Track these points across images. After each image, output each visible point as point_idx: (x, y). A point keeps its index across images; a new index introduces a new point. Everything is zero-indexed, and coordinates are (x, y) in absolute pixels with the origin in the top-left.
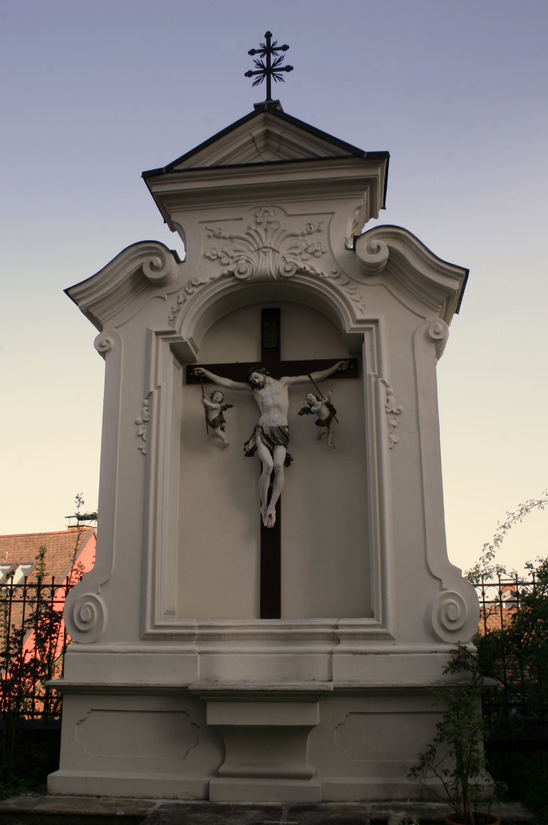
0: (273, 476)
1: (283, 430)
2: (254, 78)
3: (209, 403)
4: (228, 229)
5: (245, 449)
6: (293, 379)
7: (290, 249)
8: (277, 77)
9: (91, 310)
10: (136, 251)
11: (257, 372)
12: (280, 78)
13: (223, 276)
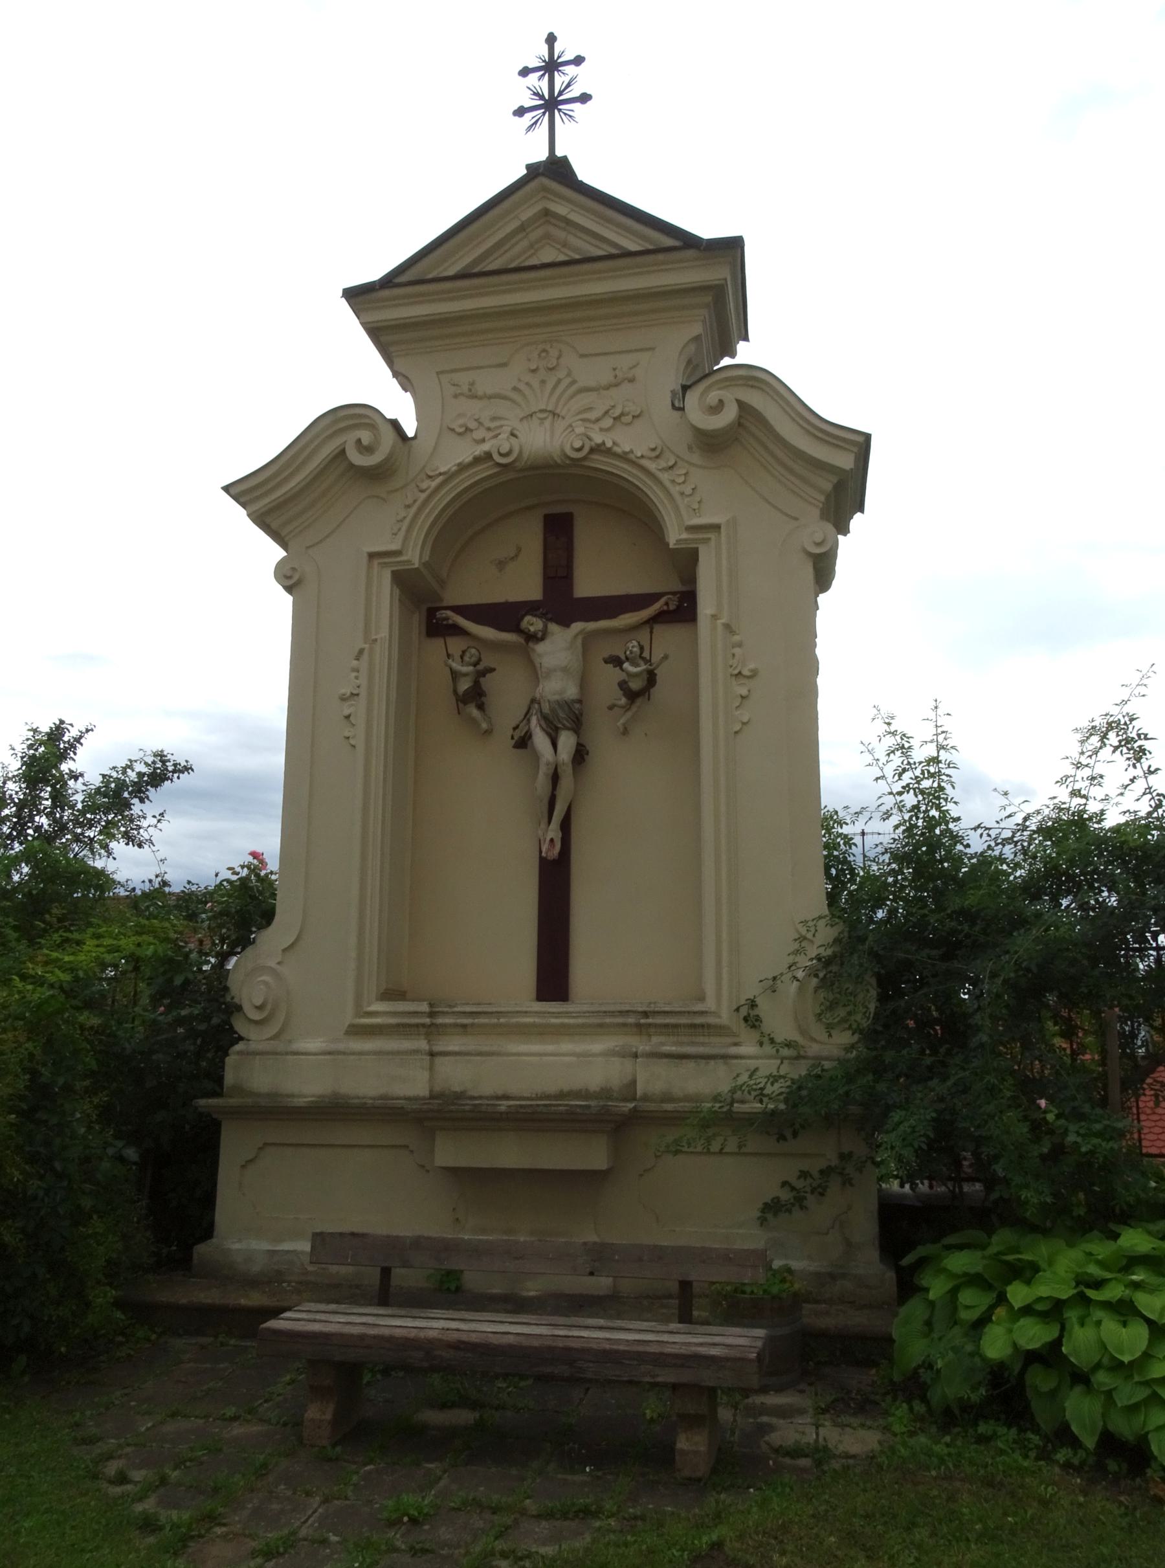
0: (555, 778)
1: (571, 705)
2: (528, 118)
3: (456, 666)
4: (488, 382)
5: (512, 738)
6: (592, 626)
7: (580, 413)
8: (565, 114)
9: (268, 520)
10: (335, 422)
11: (532, 615)
12: (570, 116)
13: (477, 460)
